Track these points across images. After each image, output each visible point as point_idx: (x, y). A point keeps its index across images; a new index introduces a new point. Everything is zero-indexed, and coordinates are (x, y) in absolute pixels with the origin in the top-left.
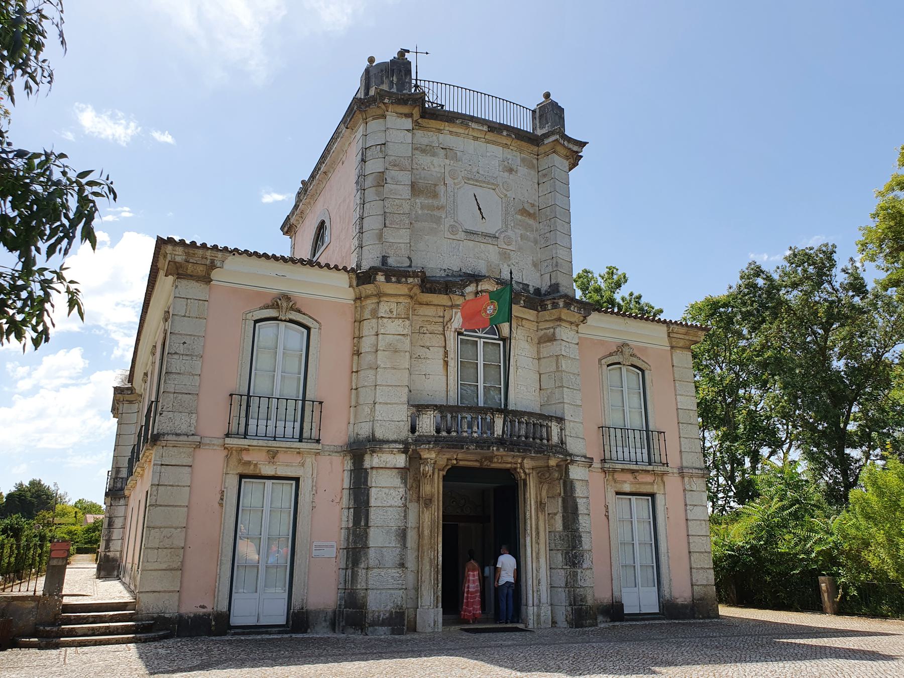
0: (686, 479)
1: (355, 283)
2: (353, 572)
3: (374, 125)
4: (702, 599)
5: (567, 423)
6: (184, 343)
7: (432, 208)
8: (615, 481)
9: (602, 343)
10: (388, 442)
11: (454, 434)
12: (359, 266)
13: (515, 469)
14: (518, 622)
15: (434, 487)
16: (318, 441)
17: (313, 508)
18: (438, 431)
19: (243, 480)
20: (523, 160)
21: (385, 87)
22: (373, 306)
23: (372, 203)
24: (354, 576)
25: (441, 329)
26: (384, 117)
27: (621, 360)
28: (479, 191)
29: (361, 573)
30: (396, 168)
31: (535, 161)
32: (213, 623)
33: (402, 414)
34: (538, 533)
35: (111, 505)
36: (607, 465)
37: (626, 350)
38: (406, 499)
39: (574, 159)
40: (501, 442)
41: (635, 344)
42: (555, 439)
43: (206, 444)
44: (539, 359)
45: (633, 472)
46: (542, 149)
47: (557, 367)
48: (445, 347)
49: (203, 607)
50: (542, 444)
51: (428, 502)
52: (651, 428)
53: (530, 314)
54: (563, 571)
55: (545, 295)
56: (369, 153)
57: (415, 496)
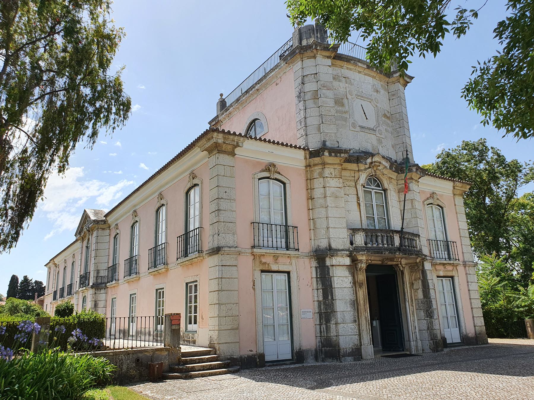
0: (467, 268)
1: (308, 157)
2: (327, 327)
3: (308, 62)
4: (480, 334)
6: (226, 192)
10: (339, 250)
13: (397, 265)
14: (403, 351)
15: (362, 277)
18: (366, 244)
19: (286, 274)
20: (382, 85)
22: (320, 170)
23: (312, 109)
24: (328, 329)
25: (354, 184)
26: (315, 57)
27: (432, 202)
29: (333, 327)
30: (325, 88)
32: (258, 360)
35: (96, 293)
41: (440, 193)
43: (243, 253)
45: (444, 264)
46: (391, 80)
47: (412, 206)
48: (357, 195)
49: (251, 351)
52: (449, 240)
56: (306, 79)
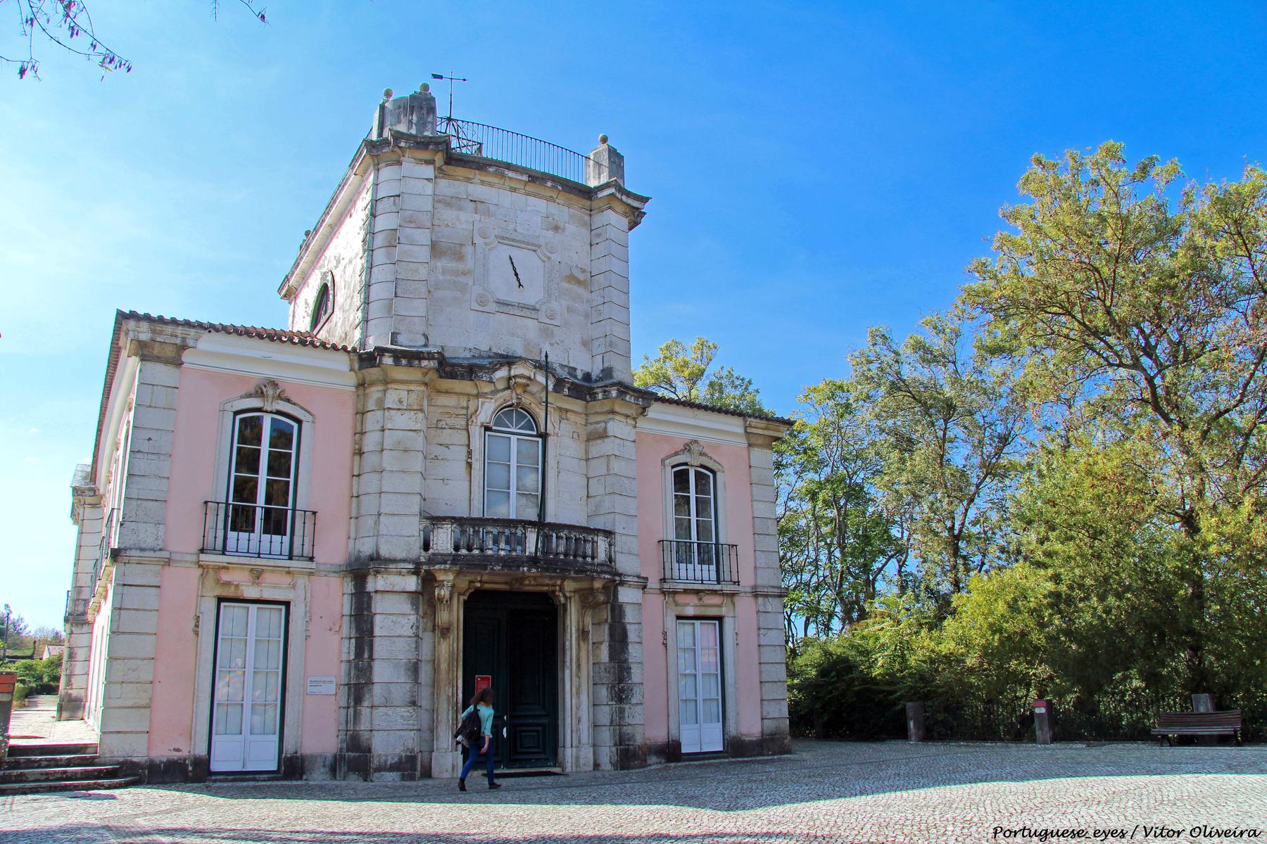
1: (356, 366)
2: (355, 712)
5: (618, 537)
7: (457, 273)
8: (677, 604)
9: (667, 439)
10: (394, 561)
11: (476, 552)
12: (363, 343)
14: (555, 766)
15: (452, 615)
16: (311, 559)
17: (307, 637)
18: (457, 548)
19: (223, 604)
21: (402, 128)
24: (357, 715)
25: (464, 423)
26: (399, 163)
28: (517, 254)
29: (365, 711)
31: (587, 218)
33: (414, 527)
34: (579, 666)
35: (72, 633)
36: (666, 586)
37: (695, 448)
38: (418, 628)
39: (635, 217)
40: (533, 561)
42: (602, 556)
44: (587, 460)
45: (697, 592)
46: (595, 204)
48: (468, 446)
49: (178, 750)
50: (586, 563)
51: (445, 631)
52: (721, 541)
53: (576, 405)
54: (608, 708)
55: (596, 381)
56: (380, 206)
57: (430, 625)
